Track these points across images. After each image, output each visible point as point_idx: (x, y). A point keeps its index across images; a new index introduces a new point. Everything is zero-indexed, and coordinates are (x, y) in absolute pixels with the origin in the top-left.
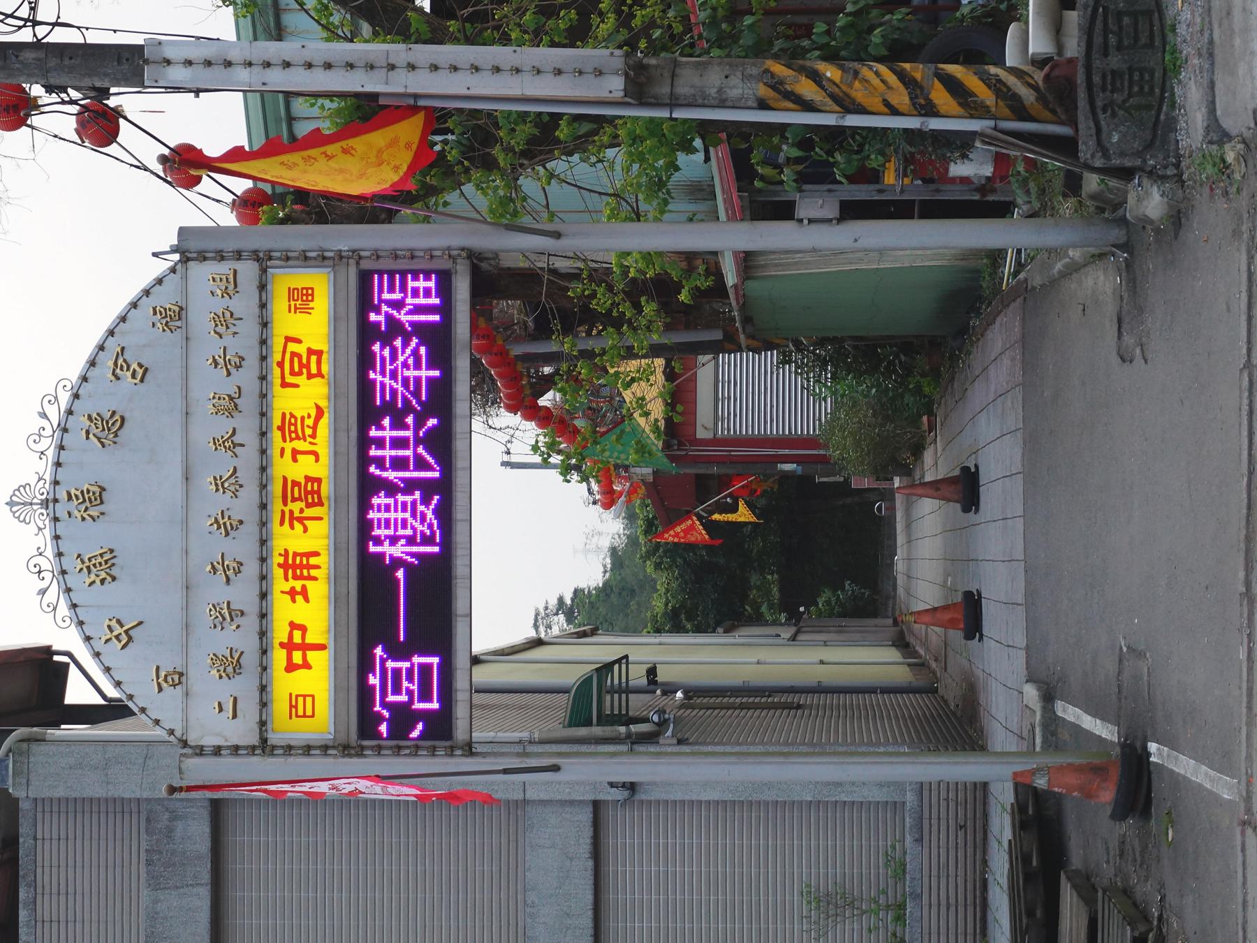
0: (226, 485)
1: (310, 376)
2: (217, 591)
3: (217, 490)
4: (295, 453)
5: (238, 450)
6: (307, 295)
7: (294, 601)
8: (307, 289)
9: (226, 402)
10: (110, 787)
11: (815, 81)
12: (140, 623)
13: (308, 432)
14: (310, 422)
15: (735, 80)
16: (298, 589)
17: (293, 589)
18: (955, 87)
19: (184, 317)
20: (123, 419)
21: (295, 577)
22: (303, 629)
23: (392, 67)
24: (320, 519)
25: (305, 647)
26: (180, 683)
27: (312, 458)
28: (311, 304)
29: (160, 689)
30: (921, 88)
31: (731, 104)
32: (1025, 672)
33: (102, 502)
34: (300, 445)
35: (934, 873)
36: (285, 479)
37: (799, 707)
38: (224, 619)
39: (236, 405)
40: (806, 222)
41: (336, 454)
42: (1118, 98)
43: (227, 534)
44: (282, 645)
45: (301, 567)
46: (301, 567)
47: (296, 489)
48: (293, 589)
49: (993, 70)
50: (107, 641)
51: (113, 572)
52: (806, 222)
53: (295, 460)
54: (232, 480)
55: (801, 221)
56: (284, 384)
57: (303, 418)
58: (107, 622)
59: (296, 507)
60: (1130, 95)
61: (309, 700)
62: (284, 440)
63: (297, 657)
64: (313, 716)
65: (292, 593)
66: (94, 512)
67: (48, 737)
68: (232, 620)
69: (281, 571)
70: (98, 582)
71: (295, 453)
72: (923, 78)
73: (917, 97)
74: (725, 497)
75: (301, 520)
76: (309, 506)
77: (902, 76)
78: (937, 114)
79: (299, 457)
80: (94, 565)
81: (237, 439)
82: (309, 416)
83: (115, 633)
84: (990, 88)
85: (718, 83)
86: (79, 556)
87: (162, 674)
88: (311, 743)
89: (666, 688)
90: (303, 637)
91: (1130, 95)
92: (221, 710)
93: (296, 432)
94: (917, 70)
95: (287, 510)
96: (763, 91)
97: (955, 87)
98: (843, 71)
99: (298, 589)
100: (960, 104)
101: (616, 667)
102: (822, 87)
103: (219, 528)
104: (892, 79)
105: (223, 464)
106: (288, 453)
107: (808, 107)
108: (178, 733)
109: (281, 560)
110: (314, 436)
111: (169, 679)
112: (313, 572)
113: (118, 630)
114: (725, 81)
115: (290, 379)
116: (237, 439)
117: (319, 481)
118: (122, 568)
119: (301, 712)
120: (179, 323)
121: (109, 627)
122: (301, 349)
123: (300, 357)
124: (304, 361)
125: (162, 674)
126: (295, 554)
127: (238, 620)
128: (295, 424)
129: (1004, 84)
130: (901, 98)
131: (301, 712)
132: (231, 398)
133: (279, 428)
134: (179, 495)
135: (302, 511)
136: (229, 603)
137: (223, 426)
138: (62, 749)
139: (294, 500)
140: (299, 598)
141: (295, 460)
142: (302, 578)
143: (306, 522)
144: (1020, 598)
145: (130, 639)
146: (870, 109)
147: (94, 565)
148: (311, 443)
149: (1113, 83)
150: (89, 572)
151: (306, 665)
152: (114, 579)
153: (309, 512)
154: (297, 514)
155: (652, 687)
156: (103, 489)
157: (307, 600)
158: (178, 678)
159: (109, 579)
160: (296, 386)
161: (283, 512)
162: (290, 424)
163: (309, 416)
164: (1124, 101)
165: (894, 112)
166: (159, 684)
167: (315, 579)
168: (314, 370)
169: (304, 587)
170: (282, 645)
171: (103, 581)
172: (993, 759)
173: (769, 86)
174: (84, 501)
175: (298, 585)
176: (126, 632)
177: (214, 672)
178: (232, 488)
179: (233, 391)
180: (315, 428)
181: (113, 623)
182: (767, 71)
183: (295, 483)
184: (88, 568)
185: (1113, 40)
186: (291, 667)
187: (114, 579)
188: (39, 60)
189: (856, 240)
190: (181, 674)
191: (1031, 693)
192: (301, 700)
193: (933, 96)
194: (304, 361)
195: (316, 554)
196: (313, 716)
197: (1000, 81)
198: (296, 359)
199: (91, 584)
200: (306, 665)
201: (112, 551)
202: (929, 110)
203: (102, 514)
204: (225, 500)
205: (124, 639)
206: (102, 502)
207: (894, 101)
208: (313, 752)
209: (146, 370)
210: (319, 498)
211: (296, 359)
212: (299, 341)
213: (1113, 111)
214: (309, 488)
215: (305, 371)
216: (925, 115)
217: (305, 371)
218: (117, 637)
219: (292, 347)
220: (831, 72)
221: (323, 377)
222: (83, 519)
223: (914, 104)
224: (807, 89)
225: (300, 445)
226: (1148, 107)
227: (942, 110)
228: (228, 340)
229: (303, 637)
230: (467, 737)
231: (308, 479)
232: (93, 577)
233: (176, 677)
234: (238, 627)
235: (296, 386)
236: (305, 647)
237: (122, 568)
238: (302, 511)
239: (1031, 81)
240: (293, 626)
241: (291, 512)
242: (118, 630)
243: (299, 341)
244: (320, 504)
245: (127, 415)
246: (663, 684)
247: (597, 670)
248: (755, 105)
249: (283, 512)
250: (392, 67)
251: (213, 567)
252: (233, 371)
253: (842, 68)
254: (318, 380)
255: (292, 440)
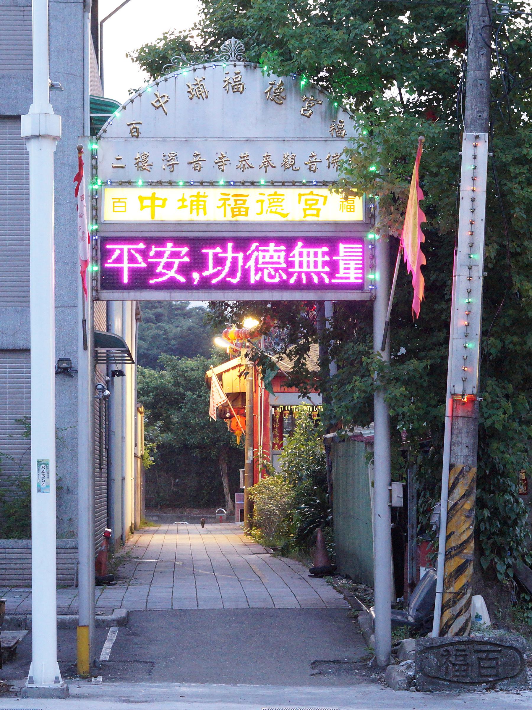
0: (244, 163)
1: (305, 210)
2: (185, 156)
3: (241, 157)
4: (262, 201)
5: (264, 169)
6: (350, 208)
7: (179, 200)
8: (354, 208)
9: (290, 162)
10: (56, 53)
11: (464, 495)
12: (166, 114)
13: (274, 209)
14: (279, 210)
15: (465, 451)
16: (185, 203)
17: (185, 200)
18: (460, 570)
19: (338, 139)
20: (282, 104)
21: (192, 201)
22: (163, 206)
23: (470, 268)
24: (225, 216)
25: (153, 206)
26: (133, 136)
27: (259, 211)
28: (345, 211)
29: (129, 125)
30: (460, 552)
31: (452, 449)
32: (132, 610)
33: (234, 92)
34: (266, 204)
35: (8, 556)
36: (247, 196)
37: (101, 469)
38: (168, 161)
39: (289, 168)
40: (390, 488)
41: (261, 224)
42: (453, 659)
43: (216, 163)
44: (154, 194)
45: (198, 205)
46: (198, 205)
47: (241, 202)
48: (185, 200)
49: (469, 591)
50: (156, 95)
51: (194, 98)
52: (390, 488)
53: (258, 201)
54: (246, 166)
55: (391, 485)
56: (300, 195)
57: (281, 206)
58: (166, 95)
59: (232, 202)
60: (454, 665)
61: (123, 209)
62: (269, 195)
63: (147, 202)
64: (114, 211)
65: (183, 200)
66: (229, 88)
67: (86, 14)
68: (168, 166)
69: (196, 194)
70: (189, 90)
71: (262, 201)
72: (465, 553)
73: (455, 550)
74: (230, 412)
75: (224, 204)
76: (232, 209)
77: (467, 542)
78: (446, 560)
79: (259, 204)
80: (199, 88)
81: (269, 168)
82: (282, 209)
83: (160, 99)
84: (460, 589)
85: (463, 442)
86: (204, 79)
87: (138, 126)
88: (99, 210)
89: (110, 383)
90: (158, 206)
91: (454, 665)
92: (118, 159)
93: (274, 202)
94: (469, 550)
95: (230, 197)
96: (459, 466)
97: (460, 570)
98: (470, 510)
99: (185, 203)
100: (451, 574)
101: (129, 358)
102: (461, 499)
103: (220, 158)
104: (465, 537)
105: (256, 160)
106: (262, 197)
107: (451, 491)
108: (104, 135)
109: (202, 194)
110: (271, 212)
111: (135, 130)
112: (195, 212)
113: (162, 101)
114: (465, 445)
115: (303, 198)
116: (269, 168)
117: (246, 215)
118: (197, 103)
119: (116, 204)
120: (335, 136)
121: (164, 96)
122: (320, 205)
123: (316, 204)
124: (313, 207)
125: (138, 126)
126: (205, 202)
127: (168, 169)
128: (278, 202)
129: (461, 598)
130: (453, 543)
131: (116, 204)
132: (292, 165)
133: (276, 192)
134: (237, 136)
135: (229, 205)
136: (177, 164)
137: (277, 161)
138: (80, 30)
139: (236, 201)
140: (180, 204)
141: (258, 201)
142: (192, 205)
143: (223, 207)
144: (176, 606)
145: (158, 108)
146: (449, 524)
147: (199, 88)
148: (267, 211)
149: (461, 656)
150: (195, 85)
151: (143, 208)
152: (191, 99)
153: (228, 210)
154: (227, 202)
155: (111, 374)
156: (241, 93)
157: (180, 208)
158: (135, 133)
159: (191, 96)
160: (299, 202)
161: (228, 195)
162: (278, 199)
163: (282, 209)
164: (450, 661)
165: (448, 537)
166: (132, 124)
167: (191, 213)
168: (308, 212)
169: (187, 206)
170: (154, 194)
171: (189, 92)
172: (91, 591)
173: (462, 470)
174: (235, 82)
175: (188, 203)
176: (161, 106)
177: (138, 156)
178: (242, 166)
179: (297, 166)
180: (276, 212)
181: (165, 99)
182: (470, 468)
183: (245, 201)
184: (197, 84)
185: (483, 655)
186: (141, 199)
187: (191, 99)
188: (481, 67)
189: (379, 516)
190: (137, 137)
191: (121, 613)
192: (123, 204)
193: (457, 559)
194: (313, 207)
195: (205, 214)
196: (114, 211)
197: (463, 595)
198: (314, 202)
199: (188, 86)
200: (143, 208)
201: (207, 97)
202: (448, 556)
203: (228, 92)
204: (235, 162)
205: (157, 105)
206: (234, 92)
207: (452, 538)
208: (94, 211)
209: (308, 117)
210: (237, 215)
211: (314, 202)
212: (325, 203)
213: (446, 655)
214: (242, 209)
215: (308, 207)
216: (446, 555)
217: (308, 207)
218: (158, 100)
219: (321, 200)
220: (468, 505)
221: (304, 217)
222: (225, 81)
223: (451, 548)
224: (459, 491)
225: (266, 204)
226: (447, 674)
227: (448, 564)
228: (325, 163)
229: (158, 206)
230: (102, 298)
231: (247, 209)
232: (192, 87)
233: (135, 134)
234: (164, 169)
235: (299, 202)
236: (153, 206)
237: (197, 103)
238: (229, 205)
239: (463, 611)
240: (165, 200)
241: (228, 199)
242: (162, 101)
243: (325, 203)
244: (233, 216)
245: (283, 106)
246: (113, 380)
247: (129, 350)
248: (452, 462)
249: (228, 195)
250: (470, 268)
251: (198, 155)
252: (308, 167)
253: (471, 510)
254: (303, 215)
255: (269, 200)
